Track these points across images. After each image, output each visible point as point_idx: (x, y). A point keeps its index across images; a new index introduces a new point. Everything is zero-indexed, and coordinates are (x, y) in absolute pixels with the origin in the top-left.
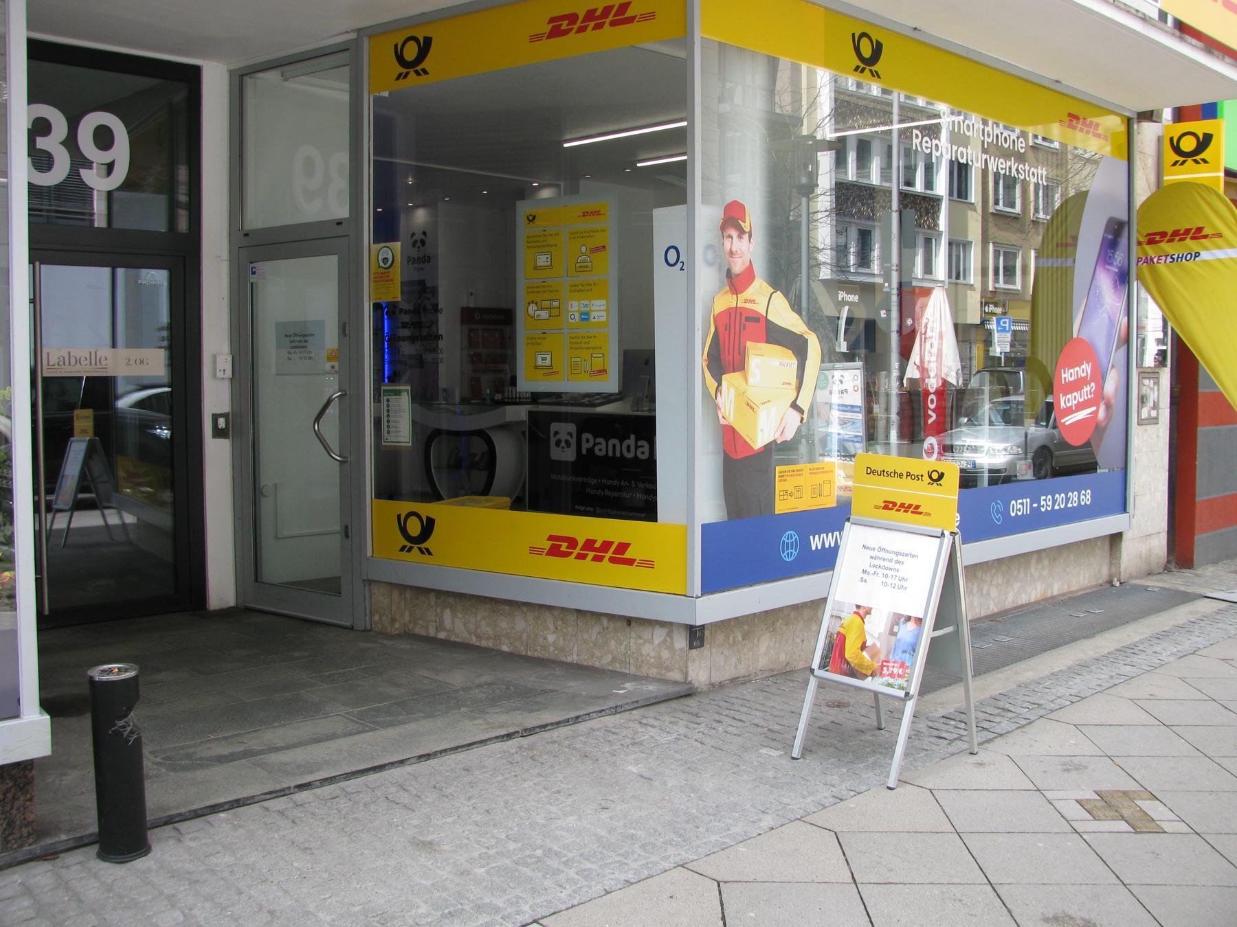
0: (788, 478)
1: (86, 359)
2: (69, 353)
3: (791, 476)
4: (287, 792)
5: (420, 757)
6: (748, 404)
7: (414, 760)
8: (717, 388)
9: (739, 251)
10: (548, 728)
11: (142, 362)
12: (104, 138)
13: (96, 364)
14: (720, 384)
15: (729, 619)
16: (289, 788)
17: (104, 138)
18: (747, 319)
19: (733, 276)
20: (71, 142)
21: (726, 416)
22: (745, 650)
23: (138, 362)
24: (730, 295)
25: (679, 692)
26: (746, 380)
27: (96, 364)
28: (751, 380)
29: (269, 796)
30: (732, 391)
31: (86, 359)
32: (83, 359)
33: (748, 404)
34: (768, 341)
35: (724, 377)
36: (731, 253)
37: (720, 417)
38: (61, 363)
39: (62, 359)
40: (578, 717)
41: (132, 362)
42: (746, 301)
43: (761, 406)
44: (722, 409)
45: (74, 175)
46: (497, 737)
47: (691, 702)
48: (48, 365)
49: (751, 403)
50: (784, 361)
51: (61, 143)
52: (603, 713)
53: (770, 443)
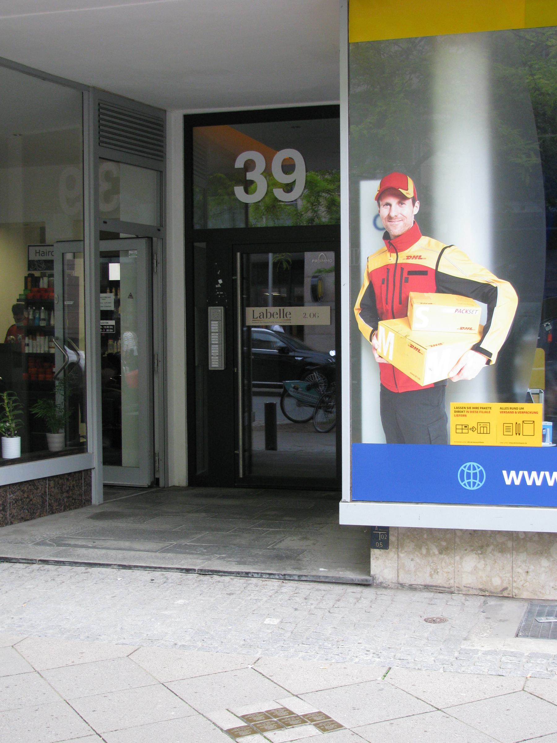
0: (467, 414)
1: (277, 314)
2: (267, 310)
3: (471, 412)
4: (34, 562)
5: (119, 565)
6: (412, 346)
7: (115, 567)
8: (372, 332)
9: (400, 216)
10: (220, 574)
11: (314, 315)
12: (288, 168)
13: (283, 317)
14: (375, 328)
15: (46, 478)
16: (36, 560)
17: (288, 168)
18: (410, 273)
19: (392, 237)
20: (267, 173)
21: (384, 355)
22: (443, 564)
23: (312, 315)
24: (388, 254)
25: (352, 580)
26: (410, 326)
27: (283, 317)
28: (415, 324)
29: (24, 561)
30: (391, 335)
31: (277, 314)
32: (275, 314)
33: (412, 346)
34: (439, 291)
35: (380, 323)
36: (390, 218)
37: (376, 356)
38: (261, 317)
39: (262, 314)
40: (247, 573)
41: (308, 315)
42: (408, 257)
43: (429, 348)
44: (379, 350)
45: (269, 192)
46: (177, 569)
47: (366, 591)
48: (254, 318)
49: (415, 345)
50: (462, 308)
51: (262, 174)
52: (272, 576)
53: (54, 364)
